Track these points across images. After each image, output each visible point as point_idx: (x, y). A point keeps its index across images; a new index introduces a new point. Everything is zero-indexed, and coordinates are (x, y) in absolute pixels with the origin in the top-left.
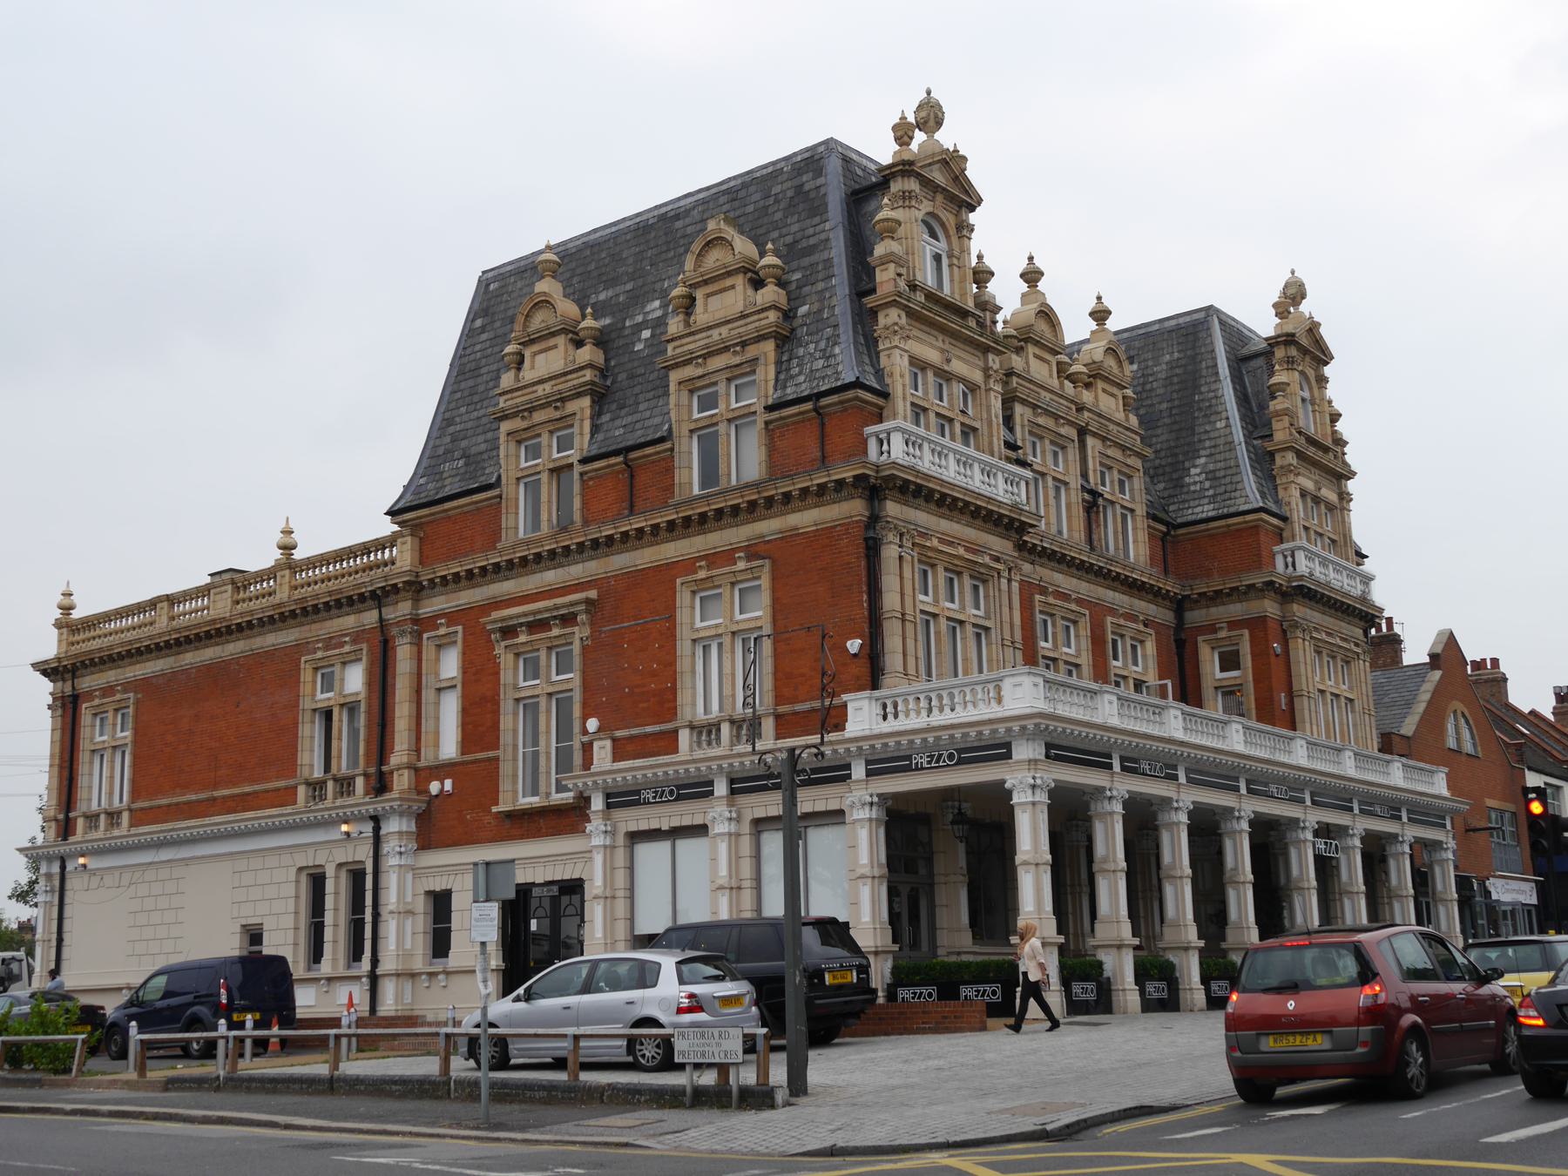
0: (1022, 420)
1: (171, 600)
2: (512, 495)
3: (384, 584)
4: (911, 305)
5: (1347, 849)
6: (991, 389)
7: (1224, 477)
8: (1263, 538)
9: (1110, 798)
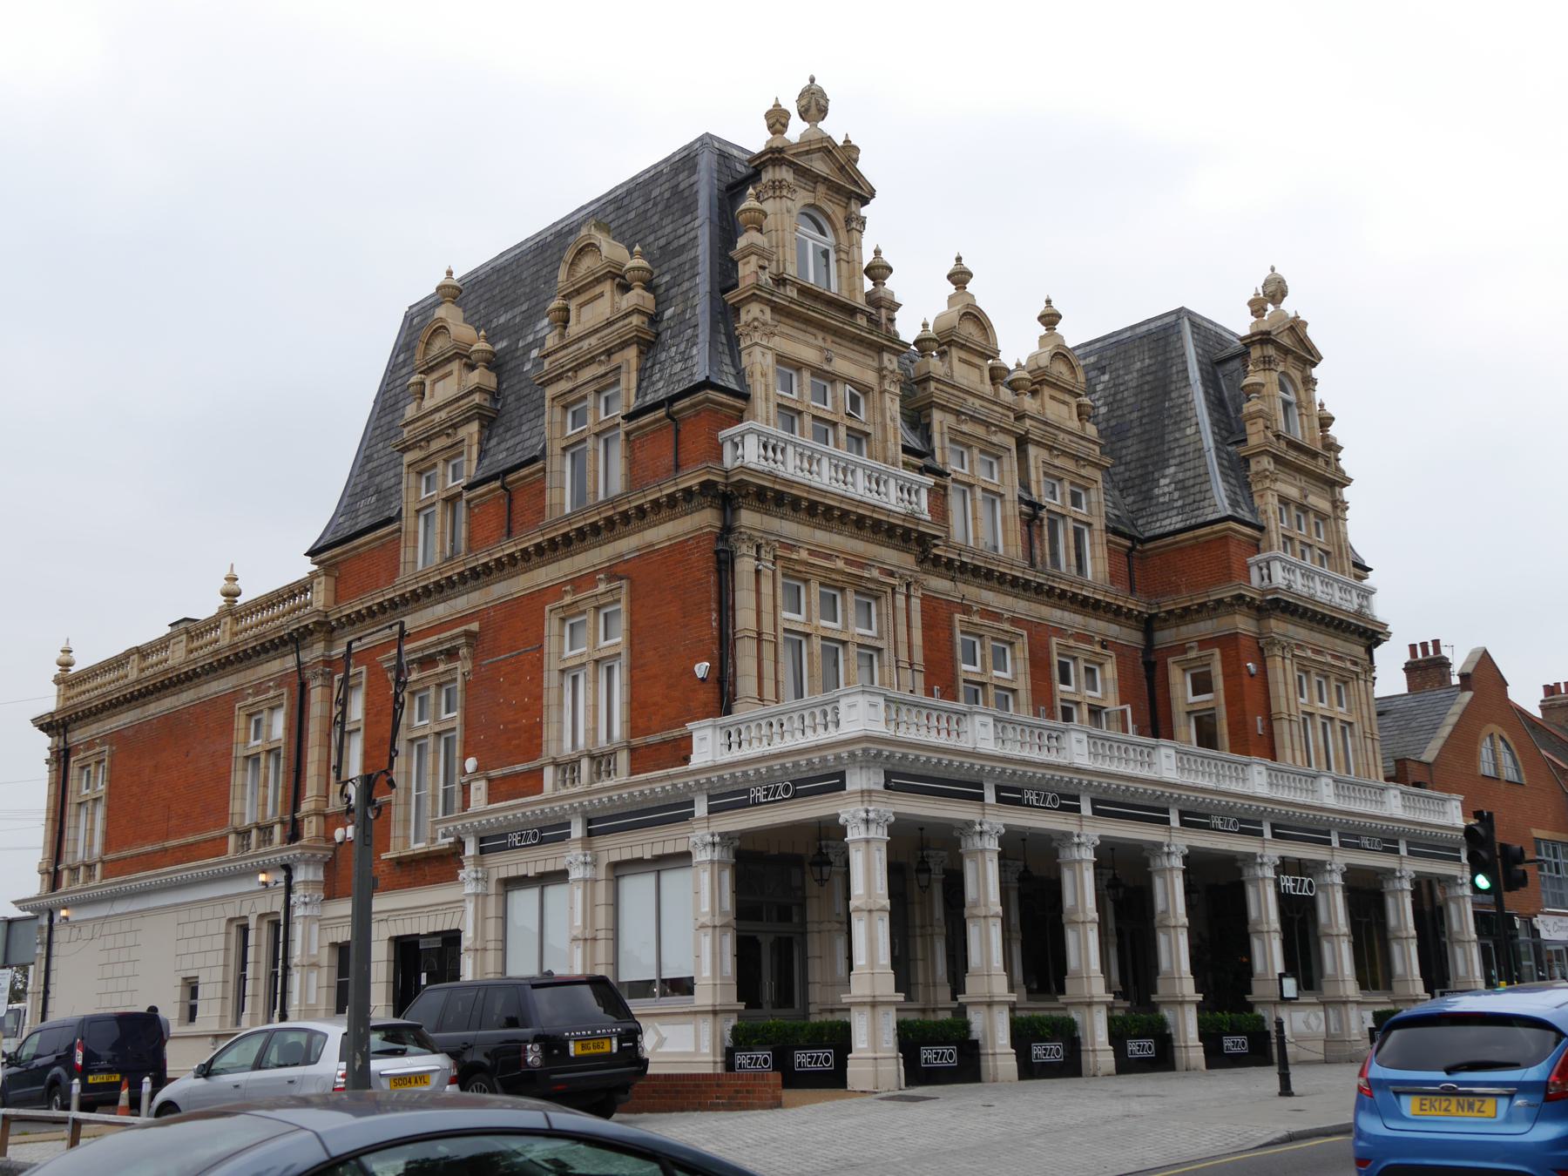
0: (942, 428)
1: (142, 652)
2: (411, 529)
3: (297, 626)
4: (774, 299)
5: (1325, 887)
6: (885, 391)
7: (1193, 486)
8: (1233, 548)
9: (981, 833)
